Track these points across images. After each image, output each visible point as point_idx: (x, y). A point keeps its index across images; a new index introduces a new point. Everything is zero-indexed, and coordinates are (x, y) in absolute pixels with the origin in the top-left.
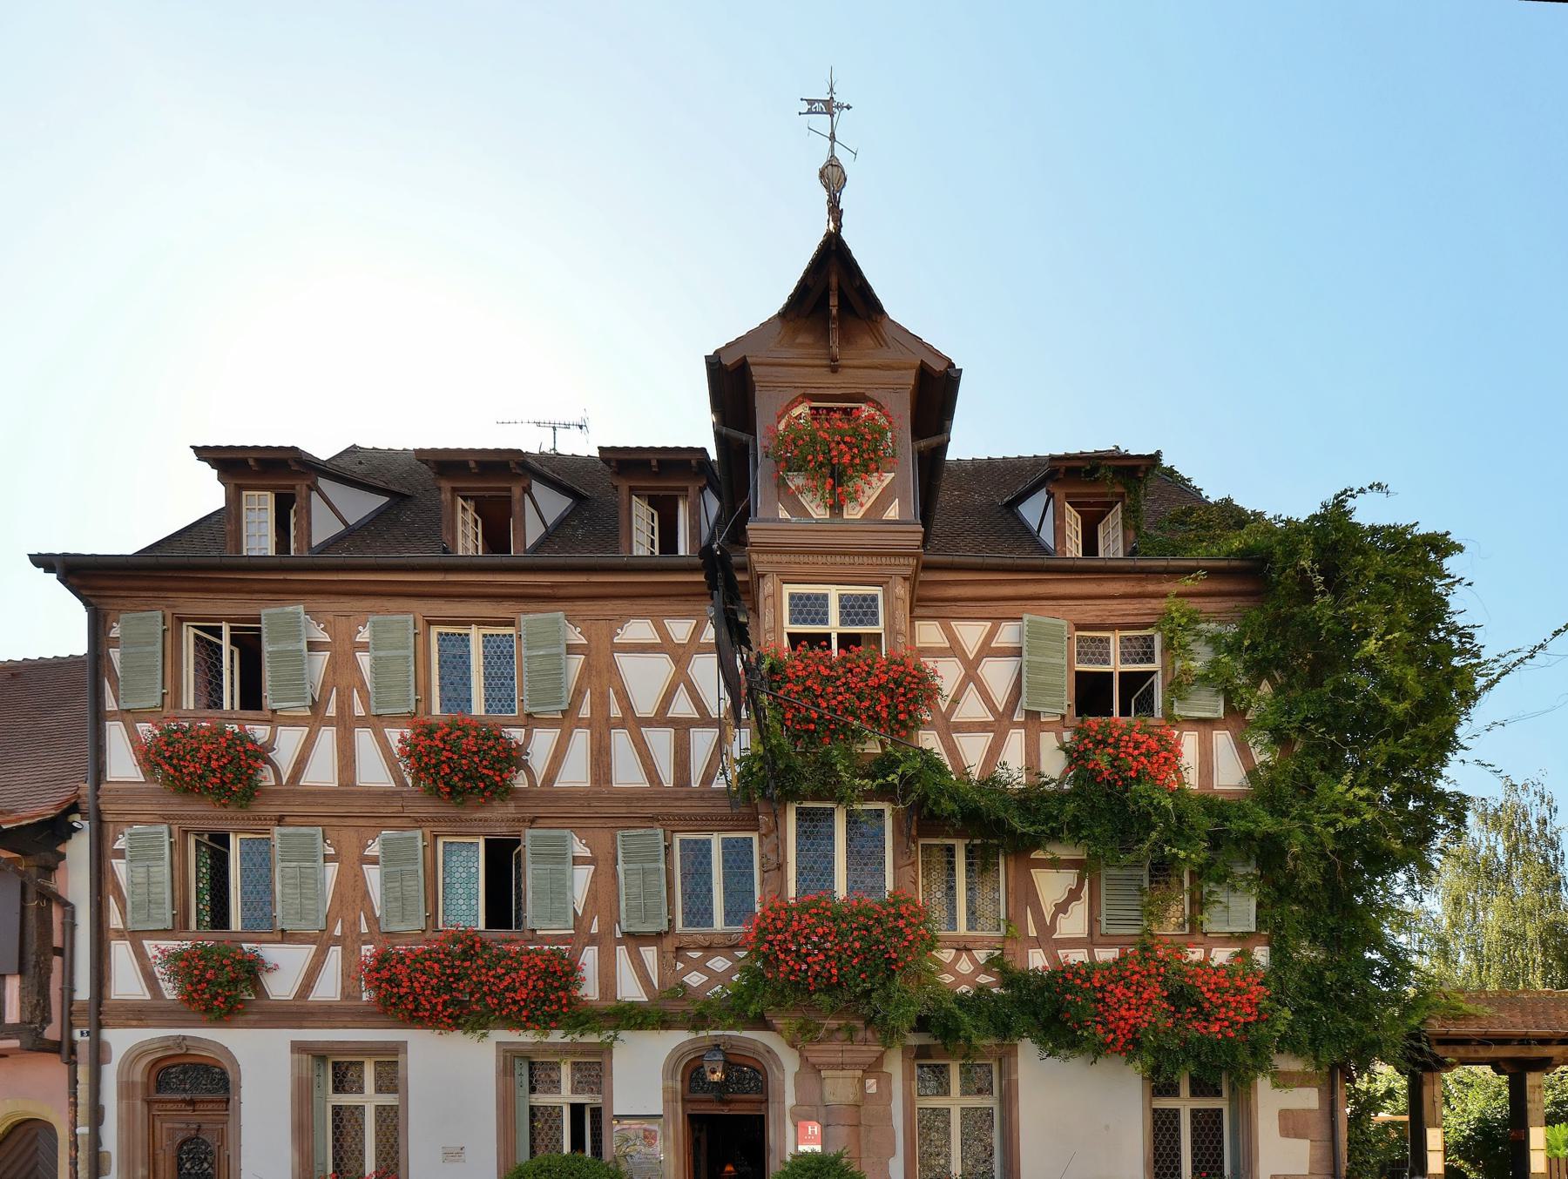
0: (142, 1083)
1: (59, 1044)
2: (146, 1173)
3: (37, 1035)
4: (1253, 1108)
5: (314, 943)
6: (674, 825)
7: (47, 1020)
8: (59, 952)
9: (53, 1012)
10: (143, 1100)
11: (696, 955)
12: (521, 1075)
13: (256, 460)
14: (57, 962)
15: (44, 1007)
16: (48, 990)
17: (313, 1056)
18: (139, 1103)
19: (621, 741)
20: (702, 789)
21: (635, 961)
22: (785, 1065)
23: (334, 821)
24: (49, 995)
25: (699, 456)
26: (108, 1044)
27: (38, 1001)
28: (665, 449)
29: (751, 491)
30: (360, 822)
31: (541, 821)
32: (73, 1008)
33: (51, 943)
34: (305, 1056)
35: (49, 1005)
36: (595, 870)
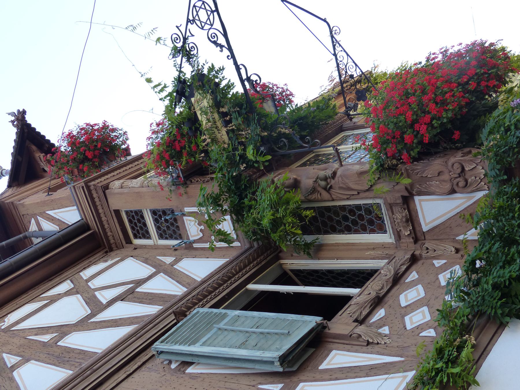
11: (381, 313)
19: (214, 9)
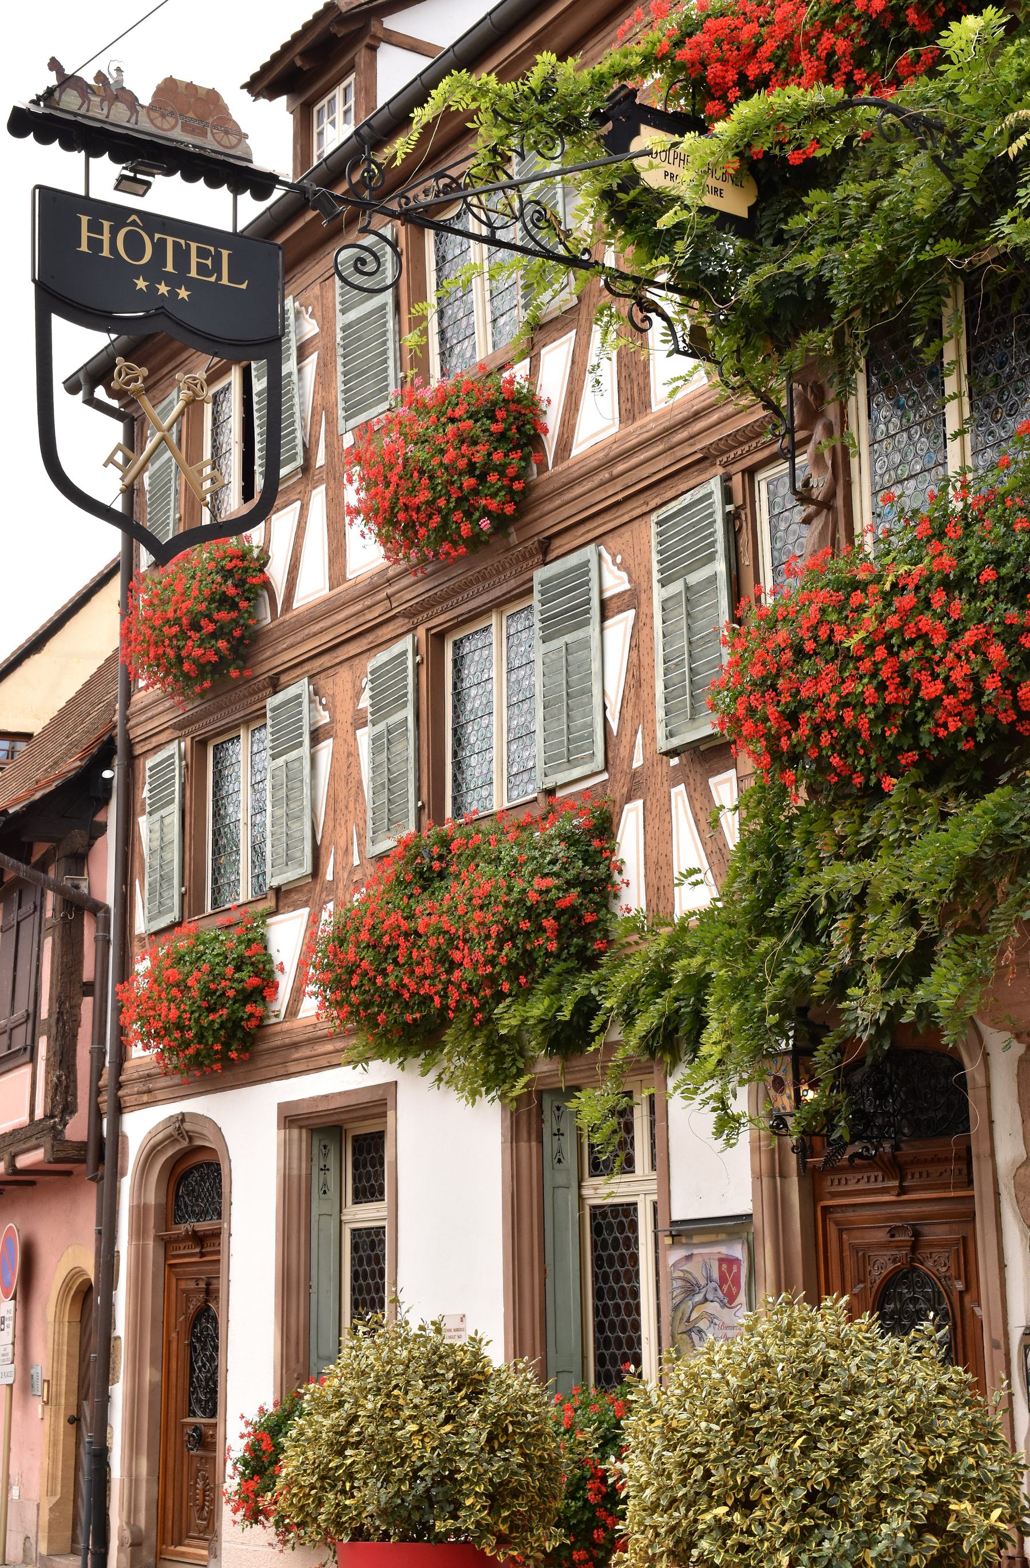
0: (157, 1206)
1: (82, 1146)
2: (158, 1377)
3: (55, 1138)
4: (225, 1190)
5: (307, 906)
6: (742, 457)
7: (69, 1108)
8: (88, 989)
9: (79, 1093)
10: (159, 1238)
12: (559, 1134)
13: (303, 54)
14: (87, 1004)
15: (67, 1087)
16: (74, 1056)
17: (313, 1131)
18: (151, 1243)
20: (623, 432)
21: (701, 816)
22: (205, 1132)
23: (326, 661)
24: (74, 1065)
25: (331, 17)
26: (125, 1137)
27: (59, 1078)
28: (297, 37)
29: (232, 161)
30: (352, 649)
31: (557, 543)
32: (122, 1078)
33: (81, 975)
34: (295, 1132)
35: (75, 1081)
36: (637, 617)
